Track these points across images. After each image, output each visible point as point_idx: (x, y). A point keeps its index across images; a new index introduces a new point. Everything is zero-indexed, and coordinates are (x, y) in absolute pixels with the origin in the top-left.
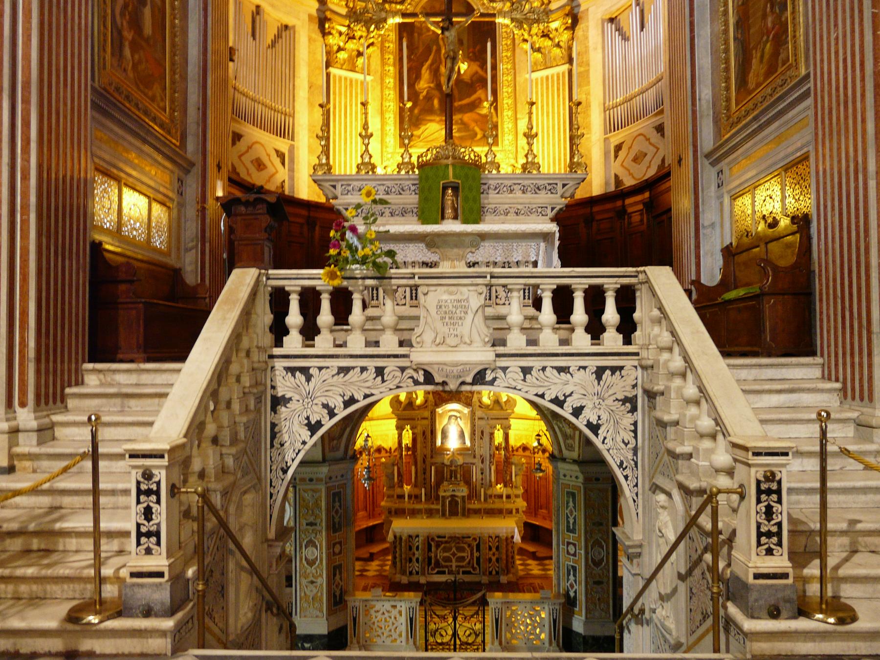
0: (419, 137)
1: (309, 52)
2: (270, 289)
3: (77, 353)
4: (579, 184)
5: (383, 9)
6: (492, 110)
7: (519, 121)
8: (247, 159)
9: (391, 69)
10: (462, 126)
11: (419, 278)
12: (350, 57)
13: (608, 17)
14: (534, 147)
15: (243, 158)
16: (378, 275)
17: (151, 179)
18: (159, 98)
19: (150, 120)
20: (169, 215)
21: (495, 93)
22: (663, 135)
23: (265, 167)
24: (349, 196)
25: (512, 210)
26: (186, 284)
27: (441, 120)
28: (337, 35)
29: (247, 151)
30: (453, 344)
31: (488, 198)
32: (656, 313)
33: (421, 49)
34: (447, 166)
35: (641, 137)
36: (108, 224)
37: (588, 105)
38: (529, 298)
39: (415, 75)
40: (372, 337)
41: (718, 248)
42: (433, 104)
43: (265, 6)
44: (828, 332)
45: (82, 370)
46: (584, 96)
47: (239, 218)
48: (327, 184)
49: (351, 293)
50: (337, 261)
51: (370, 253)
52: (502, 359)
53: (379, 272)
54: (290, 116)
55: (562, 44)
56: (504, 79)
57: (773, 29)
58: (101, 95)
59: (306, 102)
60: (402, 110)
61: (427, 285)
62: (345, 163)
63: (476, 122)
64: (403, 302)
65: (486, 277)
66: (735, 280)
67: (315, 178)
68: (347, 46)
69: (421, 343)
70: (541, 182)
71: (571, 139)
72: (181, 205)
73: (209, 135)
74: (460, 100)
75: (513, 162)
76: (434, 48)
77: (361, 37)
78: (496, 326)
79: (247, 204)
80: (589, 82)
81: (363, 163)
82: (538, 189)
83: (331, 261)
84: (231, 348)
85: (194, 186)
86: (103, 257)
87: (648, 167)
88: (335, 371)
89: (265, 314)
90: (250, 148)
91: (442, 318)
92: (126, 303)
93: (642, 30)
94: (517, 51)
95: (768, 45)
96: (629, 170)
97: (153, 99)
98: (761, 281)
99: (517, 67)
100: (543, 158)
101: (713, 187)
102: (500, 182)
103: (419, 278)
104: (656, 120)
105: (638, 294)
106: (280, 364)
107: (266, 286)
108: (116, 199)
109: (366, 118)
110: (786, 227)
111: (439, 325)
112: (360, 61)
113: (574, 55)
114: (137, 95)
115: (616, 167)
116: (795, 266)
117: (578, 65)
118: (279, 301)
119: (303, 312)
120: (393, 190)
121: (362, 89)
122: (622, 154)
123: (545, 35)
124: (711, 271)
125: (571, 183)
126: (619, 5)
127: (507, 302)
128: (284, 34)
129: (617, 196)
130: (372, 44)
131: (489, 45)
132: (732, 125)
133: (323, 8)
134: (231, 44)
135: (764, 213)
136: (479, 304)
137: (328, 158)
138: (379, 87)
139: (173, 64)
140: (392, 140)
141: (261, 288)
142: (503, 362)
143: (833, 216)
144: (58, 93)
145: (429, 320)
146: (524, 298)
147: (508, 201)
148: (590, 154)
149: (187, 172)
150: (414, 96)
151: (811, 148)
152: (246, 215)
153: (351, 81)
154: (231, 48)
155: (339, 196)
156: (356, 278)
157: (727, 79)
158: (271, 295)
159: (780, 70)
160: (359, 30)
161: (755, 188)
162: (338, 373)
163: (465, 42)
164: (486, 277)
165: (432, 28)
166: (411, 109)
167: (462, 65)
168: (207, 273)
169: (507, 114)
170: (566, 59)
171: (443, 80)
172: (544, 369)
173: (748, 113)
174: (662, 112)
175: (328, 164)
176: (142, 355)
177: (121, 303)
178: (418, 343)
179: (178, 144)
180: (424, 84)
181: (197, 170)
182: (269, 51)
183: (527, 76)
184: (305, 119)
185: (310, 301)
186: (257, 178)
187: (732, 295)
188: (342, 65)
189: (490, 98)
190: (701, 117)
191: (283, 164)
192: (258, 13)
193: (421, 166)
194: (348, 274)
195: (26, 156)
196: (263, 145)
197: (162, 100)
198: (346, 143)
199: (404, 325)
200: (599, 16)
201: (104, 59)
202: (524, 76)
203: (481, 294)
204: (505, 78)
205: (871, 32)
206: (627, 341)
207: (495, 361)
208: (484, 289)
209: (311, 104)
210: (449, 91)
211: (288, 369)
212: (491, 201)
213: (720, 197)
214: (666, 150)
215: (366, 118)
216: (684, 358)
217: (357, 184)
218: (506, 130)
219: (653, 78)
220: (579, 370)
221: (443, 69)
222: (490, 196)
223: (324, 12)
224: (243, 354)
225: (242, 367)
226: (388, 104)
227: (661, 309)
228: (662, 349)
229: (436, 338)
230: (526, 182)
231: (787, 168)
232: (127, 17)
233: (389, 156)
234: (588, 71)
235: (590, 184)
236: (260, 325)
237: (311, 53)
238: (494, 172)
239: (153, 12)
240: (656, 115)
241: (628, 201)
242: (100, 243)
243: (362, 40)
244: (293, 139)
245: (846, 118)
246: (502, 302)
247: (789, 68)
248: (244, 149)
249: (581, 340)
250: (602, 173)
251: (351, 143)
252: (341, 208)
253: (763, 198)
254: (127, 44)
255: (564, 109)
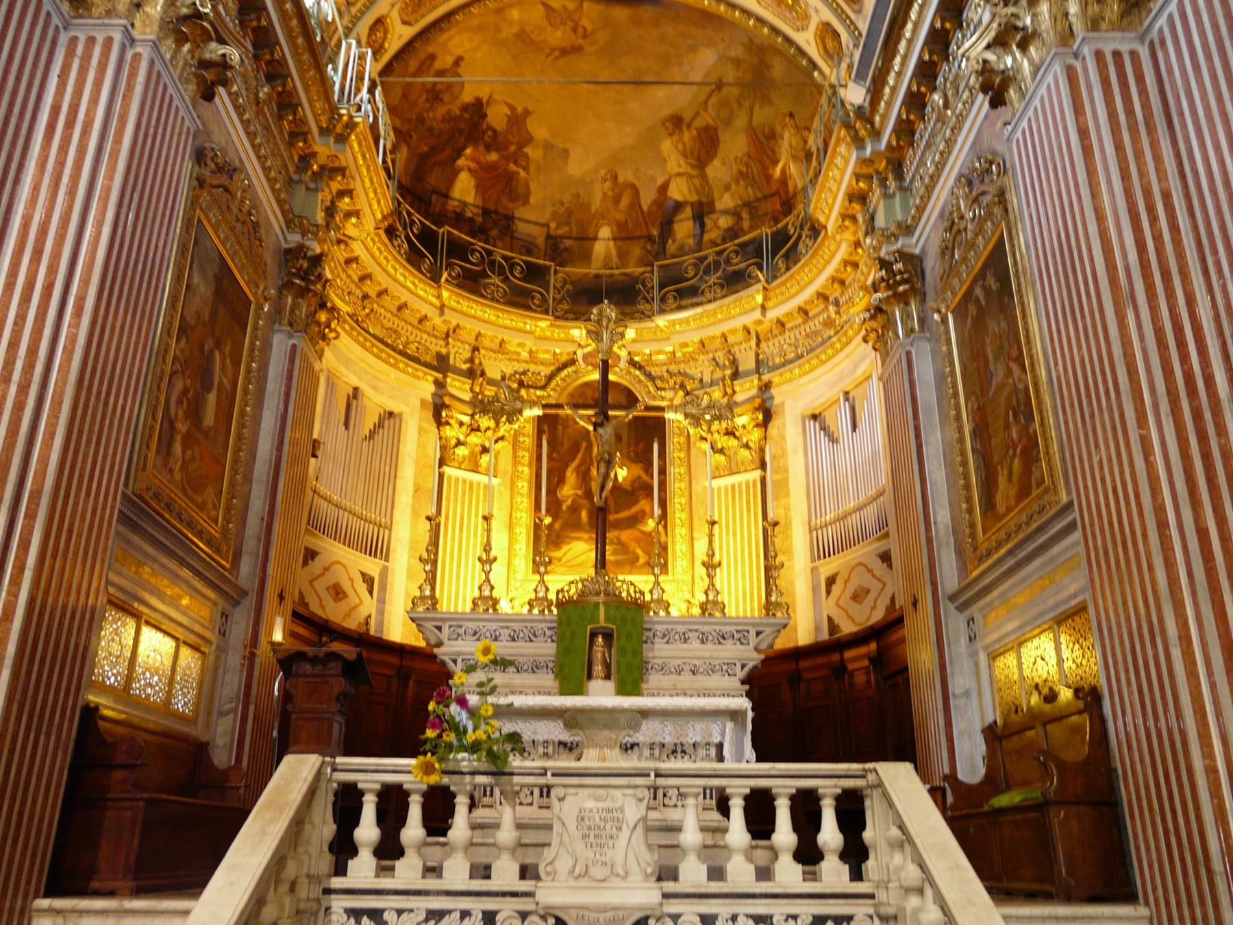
0: (560, 560)
1: (419, 446)
2: (335, 785)
3: (28, 883)
4: (779, 631)
5: (520, 399)
6: (661, 528)
7: (696, 543)
8: (320, 585)
9: (526, 471)
10: (618, 547)
11: (553, 775)
12: (472, 453)
13: (810, 412)
14: (717, 582)
15: (315, 584)
16: (493, 769)
17: (184, 613)
18: (210, 505)
19: (194, 535)
20: (203, 664)
21: (663, 504)
22: (890, 566)
23: (345, 596)
24: (460, 642)
25: (687, 668)
26: (213, 764)
27: (591, 538)
28: (456, 426)
29: (322, 575)
30: (599, 877)
31: (653, 650)
32: (895, 832)
33: (566, 446)
34: (597, 605)
35: (861, 568)
36: (113, 679)
37: (789, 524)
38: (711, 798)
39: (557, 477)
40: (482, 856)
41: (978, 727)
42: (579, 517)
43: (364, 387)
44: (1151, 867)
45: (31, 911)
46: (782, 512)
47: (301, 680)
48: (429, 625)
49: (454, 796)
50: (436, 746)
51: (485, 737)
52: (672, 901)
53: (496, 765)
54: (385, 527)
55: (751, 444)
56: (676, 486)
57: (1020, 440)
58: (134, 504)
59: (408, 510)
60: (537, 527)
61: (565, 786)
62: (457, 595)
63: (638, 541)
64: (529, 800)
65: (648, 775)
66: (1006, 780)
67: (413, 615)
68: (469, 440)
69: (553, 875)
70: (725, 629)
71: (767, 569)
72: (222, 650)
73: (272, 554)
74: (617, 512)
75: (688, 596)
76: (584, 445)
77: (488, 429)
78: (663, 842)
79: (315, 660)
80: (788, 494)
81: (481, 597)
82: (723, 638)
83: (428, 746)
84: (268, 881)
85: (243, 623)
86: (96, 725)
87: (874, 608)
88: (422, 916)
89: (324, 823)
90: (326, 569)
91: (585, 836)
92: (122, 799)
93: (854, 429)
94: (693, 451)
95: (1016, 461)
96: (846, 612)
97: (202, 507)
98: (1045, 783)
99: (693, 471)
100: (730, 593)
101: (963, 640)
102: (669, 627)
103: (553, 775)
104: (880, 546)
105: (867, 803)
106: (339, 904)
107: (330, 780)
108: (131, 643)
109: (488, 536)
110: (1068, 704)
111: (579, 846)
112: (485, 459)
113: (768, 459)
114: (181, 501)
115: (829, 607)
116: (1088, 762)
117: (774, 471)
118: (347, 803)
119: (381, 819)
120: (522, 635)
121: (485, 495)
122: (837, 589)
123: (730, 433)
124: (971, 762)
125: (768, 630)
126: (823, 400)
127: (680, 803)
128: (386, 422)
129: (832, 647)
130: (502, 438)
131: (656, 446)
132: (981, 560)
133: (442, 392)
134: (315, 436)
135: (1037, 680)
136: (638, 816)
137: (433, 589)
138: (509, 492)
139: (236, 461)
140: (523, 563)
141: (323, 785)
142: (673, 907)
143: (1130, 693)
144: (76, 504)
145: (566, 838)
146: (705, 798)
147: (681, 654)
148: (793, 588)
149: (236, 603)
150: (554, 507)
151: (1088, 596)
152: (312, 675)
153: (471, 484)
154: (315, 441)
155: (445, 641)
156: (462, 773)
157: (969, 499)
158: (336, 795)
159: (1035, 493)
160: (485, 422)
161: (1020, 644)
162: (427, 920)
163: (625, 438)
164: (648, 775)
165: (582, 423)
166: (550, 526)
167: (619, 470)
168: (246, 749)
169: (679, 532)
170: (758, 463)
171: (595, 487)
172: (734, 918)
173: (1000, 545)
174: (887, 535)
175: (433, 597)
176: (132, 884)
177: (115, 800)
178: (548, 874)
179: (228, 566)
180: (568, 491)
181: (250, 602)
182: (366, 443)
183: (707, 484)
184: (406, 534)
185: (392, 803)
186: (333, 612)
187: (1003, 800)
188: (461, 463)
189: (657, 511)
190: (939, 548)
191: (371, 592)
192: (355, 397)
193: (560, 604)
194: (451, 766)
195: (14, 589)
196: (345, 567)
197: (215, 507)
198: (459, 566)
199: (530, 837)
200: (798, 412)
201: (146, 456)
202: (703, 483)
203: (641, 800)
204: (677, 485)
205: (1142, 458)
206: (857, 875)
207: (661, 905)
208: (646, 794)
209: (415, 513)
210: (601, 504)
211: (351, 912)
212: (657, 653)
213: (973, 655)
214: (895, 585)
215: (488, 536)
216: (942, 908)
217: (472, 625)
218: (679, 553)
219: (872, 492)
220: (786, 920)
221: (594, 472)
222: (656, 646)
223: (441, 397)
224: (284, 888)
225: (282, 908)
226: (519, 515)
227: (902, 827)
228: (908, 890)
229: (574, 866)
230: (706, 629)
231: (1060, 621)
232: (185, 405)
233: (518, 584)
234: (787, 480)
235: (795, 630)
236: (315, 839)
237: (421, 447)
238: (662, 613)
239: (218, 397)
240: (879, 539)
241: (849, 654)
242: (97, 708)
243: (489, 433)
244: (387, 559)
245: (1128, 562)
246: (674, 801)
247: (1047, 490)
248: (318, 572)
249: (789, 873)
250: (811, 615)
251: (467, 566)
252: (447, 659)
253: (1033, 660)
254: (178, 438)
255: (756, 528)
